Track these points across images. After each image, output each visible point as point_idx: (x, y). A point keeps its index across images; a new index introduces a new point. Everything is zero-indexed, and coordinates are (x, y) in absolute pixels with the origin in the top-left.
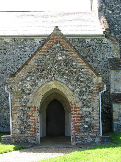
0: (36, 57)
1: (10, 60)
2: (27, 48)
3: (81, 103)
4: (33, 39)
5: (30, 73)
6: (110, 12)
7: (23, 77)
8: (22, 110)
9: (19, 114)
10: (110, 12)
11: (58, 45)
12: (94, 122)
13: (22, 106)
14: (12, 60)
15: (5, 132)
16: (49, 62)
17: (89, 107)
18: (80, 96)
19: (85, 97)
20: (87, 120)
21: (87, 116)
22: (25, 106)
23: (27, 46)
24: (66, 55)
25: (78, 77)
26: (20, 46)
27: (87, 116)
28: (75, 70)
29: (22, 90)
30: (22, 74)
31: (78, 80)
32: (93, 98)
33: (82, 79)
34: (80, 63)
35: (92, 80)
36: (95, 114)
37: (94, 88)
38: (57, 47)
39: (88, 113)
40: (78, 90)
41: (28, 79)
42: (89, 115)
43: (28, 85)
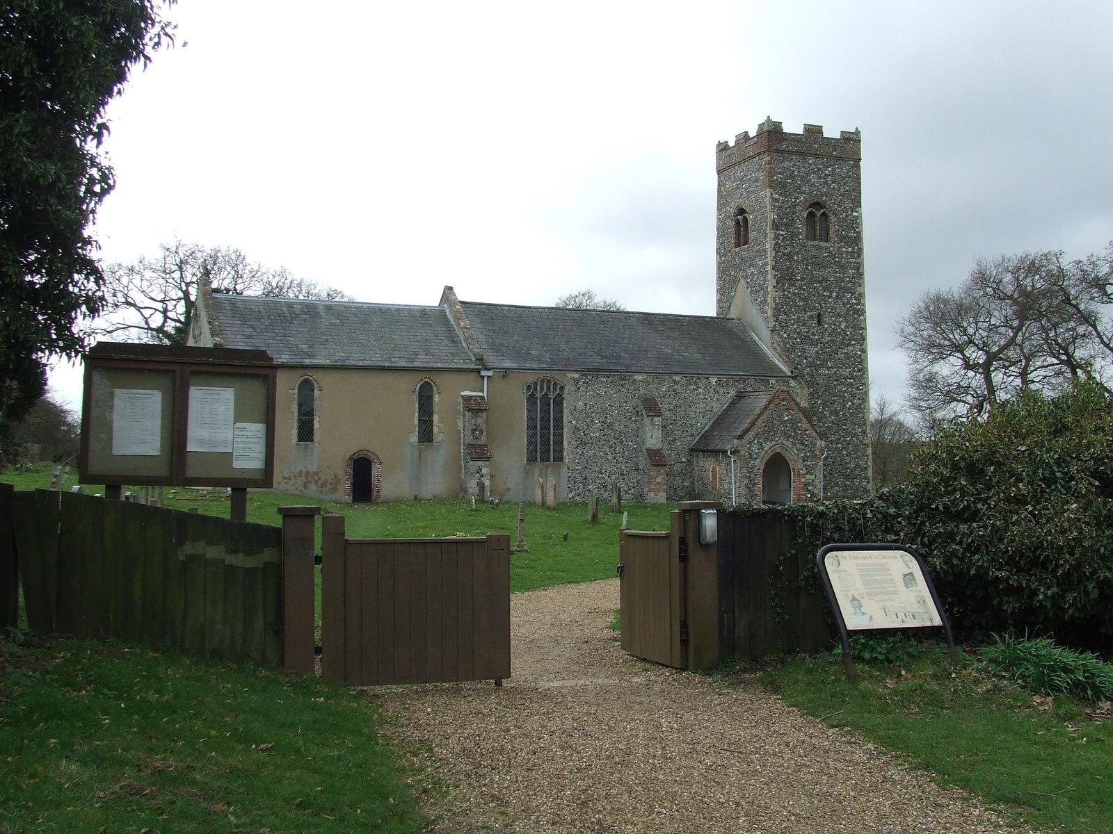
0: (764, 417)
1: (680, 407)
2: (701, 390)
3: (804, 469)
4: (708, 378)
5: (757, 434)
6: (785, 335)
7: (750, 439)
8: (749, 477)
9: (746, 481)
10: (785, 335)
11: (784, 403)
12: (816, 491)
13: (749, 472)
14: (683, 407)
15: (314, 592)
16: (775, 422)
17: (812, 474)
18: (804, 461)
19: (809, 463)
20: (810, 488)
21: (809, 484)
22: (752, 472)
23: (701, 388)
24: (792, 415)
25: (802, 441)
26: (692, 387)
27: (809, 484)
28: (800, 432)
29: (749, 454)
30: (750, 435)
31: (803, 444)
32: (816, 464)
33: (806, 443)
34: (804, 424)
35: (815, 444)
36: (817, 482)
37: (817, 452)
38: (784, 405)
39: (811, 481)
40: (802, 455)
41: (756, 442)
42: (812, 484)
43: (755, 448)
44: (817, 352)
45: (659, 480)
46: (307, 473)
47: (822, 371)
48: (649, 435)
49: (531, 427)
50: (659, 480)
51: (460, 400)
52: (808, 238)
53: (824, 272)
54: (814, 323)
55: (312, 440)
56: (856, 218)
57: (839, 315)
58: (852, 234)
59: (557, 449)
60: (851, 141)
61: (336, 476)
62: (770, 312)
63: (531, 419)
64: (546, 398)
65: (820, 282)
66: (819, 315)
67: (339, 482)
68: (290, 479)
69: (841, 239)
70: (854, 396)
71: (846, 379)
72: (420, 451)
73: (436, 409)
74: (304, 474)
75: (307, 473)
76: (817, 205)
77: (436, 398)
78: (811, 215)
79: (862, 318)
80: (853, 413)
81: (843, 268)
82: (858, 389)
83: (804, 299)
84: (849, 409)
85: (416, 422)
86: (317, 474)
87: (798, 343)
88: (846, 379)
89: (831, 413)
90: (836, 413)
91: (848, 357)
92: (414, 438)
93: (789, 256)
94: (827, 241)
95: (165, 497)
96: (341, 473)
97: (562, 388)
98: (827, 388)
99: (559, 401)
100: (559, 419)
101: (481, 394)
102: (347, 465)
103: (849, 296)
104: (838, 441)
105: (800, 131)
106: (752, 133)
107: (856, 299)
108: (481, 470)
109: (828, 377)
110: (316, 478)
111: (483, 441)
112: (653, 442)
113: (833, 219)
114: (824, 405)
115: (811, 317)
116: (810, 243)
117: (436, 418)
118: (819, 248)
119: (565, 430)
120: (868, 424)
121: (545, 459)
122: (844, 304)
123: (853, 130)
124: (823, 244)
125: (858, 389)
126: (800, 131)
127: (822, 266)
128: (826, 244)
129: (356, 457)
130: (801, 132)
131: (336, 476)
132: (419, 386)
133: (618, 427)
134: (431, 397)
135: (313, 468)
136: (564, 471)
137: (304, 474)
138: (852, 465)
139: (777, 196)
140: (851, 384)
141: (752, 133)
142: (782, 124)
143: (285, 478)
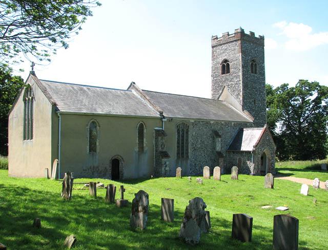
46: (94, 167)
48: (217, 145)
51: (154, 131)
61: (106, 168)
62: (241, 99)
63: (178, 140)
64: (183, 130)
67: (107, 171)
68: (86, 170)
72: (139, 155)
73: (145, 135)
74: (92, 168)
75: (94, 167)
77: (145, 131)
83: (251, 95)
86: (98, 167)
91: (262, 116)
93: (247, 78)
97: (188, 126)
99: (187, 133)
101: (161, 129)
106: (289, 87)
108: (166, 163)
110: (97, 169)
117: (145, 140)
118: (254, 76)
119: (189, 144)
120: (77, 15)
127: (255, 83)
131: (106, 168)
134: (143, 130)
135: (96, 165)
136: (189, 161)
137: (92, 168)
141: (289, 87)
143: (84, 170)
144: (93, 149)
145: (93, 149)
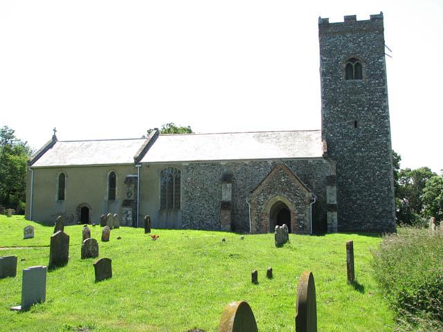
0: (267, 180)
20: (301, 222)
30: (258, 191)
36: (307, 219)
43: (261, 199)
44: (354, 143)
45: (226, 218)
47: (358, 154)
49: (163, 191)
50: (226, 218)
52: (347, 79)
53: (358, 97)
54: (352, 127)
55: (64, 199)
56: (381, 63)
57: (370, 120)
58: (378, 72)
59: (177, 201)
60: (376, 23)
65: (356, 103)
66: (356, 122)
69: (371, 76)
70: (381, 168)
71: (375, 158)
72: (109, 204)
73: (117, 183)
76: (353, 60)
77: (117, 179)
78: (348, 65)
79: (386, 121)
80: (381, 178)
81: (372, 92)
82: (384, 163)
84: (378, 176)
85: (107, 190)
87: (340, 139)
88: (375, 158)
89: (365, 179)
90: (368, 178)
92: (106, 198)
93: (334, 90)
94: (361, 78)
95: (74, 233)
96: (75, 215)
98: (362, 164)
100: (178, 188)
102: (77, 210)
103: (376, 108)
104: (370, 195)
105: (342, 20)
107: (382, 110)
109: (363, 157)
111: (132, 198)
112: (226, 197)
113: (364, 65)
114: (360, 174)
115: (349, 123)
116: (348, 81)
117: (116, 188)
118: (355, 84)
121: (170, 206)
122: (373, 114)
123: (379, 13)
124: (357, 81)
125: (384, 163)
126: (342, 20)
128: (360, 81)
129: (82, 206)
130: (343, 21)
132: (109, 173)
133: (211, 190)
138: (381, 210)
139: (325, 58)
140: (378, 161)
142: (322, 17)
144: (61, 197)
145: (61, 197)
